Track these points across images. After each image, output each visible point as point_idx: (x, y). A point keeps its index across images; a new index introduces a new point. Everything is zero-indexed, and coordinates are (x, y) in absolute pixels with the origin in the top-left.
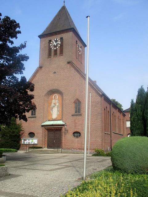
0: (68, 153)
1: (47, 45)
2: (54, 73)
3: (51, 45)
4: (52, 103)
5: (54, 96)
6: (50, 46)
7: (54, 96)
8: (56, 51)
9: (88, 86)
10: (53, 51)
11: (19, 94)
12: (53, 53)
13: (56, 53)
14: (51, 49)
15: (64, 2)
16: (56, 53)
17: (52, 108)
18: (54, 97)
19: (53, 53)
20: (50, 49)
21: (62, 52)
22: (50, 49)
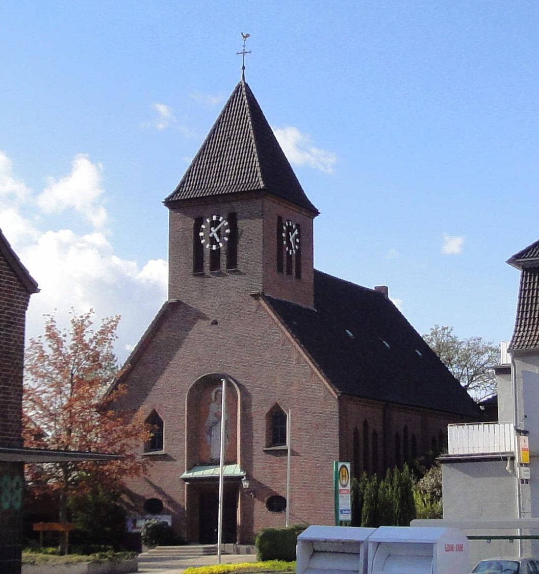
0: (149, 455)
1: (190, 235)
2: (212, 324)
3: (201, 234)
4: (211, 414)
5: (213, 394)
6: (197, 239)
7: (213, 394)
8: (215, 255)
9: (191, 545)
10: (207, 255)
11: (118, 491)
12: (207, 263)
13: (215, 265)
14: (202, 246)
15: (244, 68)
16: (215, 265)
17: (211, 429)
18: (216, 393)
19: (207, 263)
20: (198, 248)
21: (232, 262)
22: (198, 248)
